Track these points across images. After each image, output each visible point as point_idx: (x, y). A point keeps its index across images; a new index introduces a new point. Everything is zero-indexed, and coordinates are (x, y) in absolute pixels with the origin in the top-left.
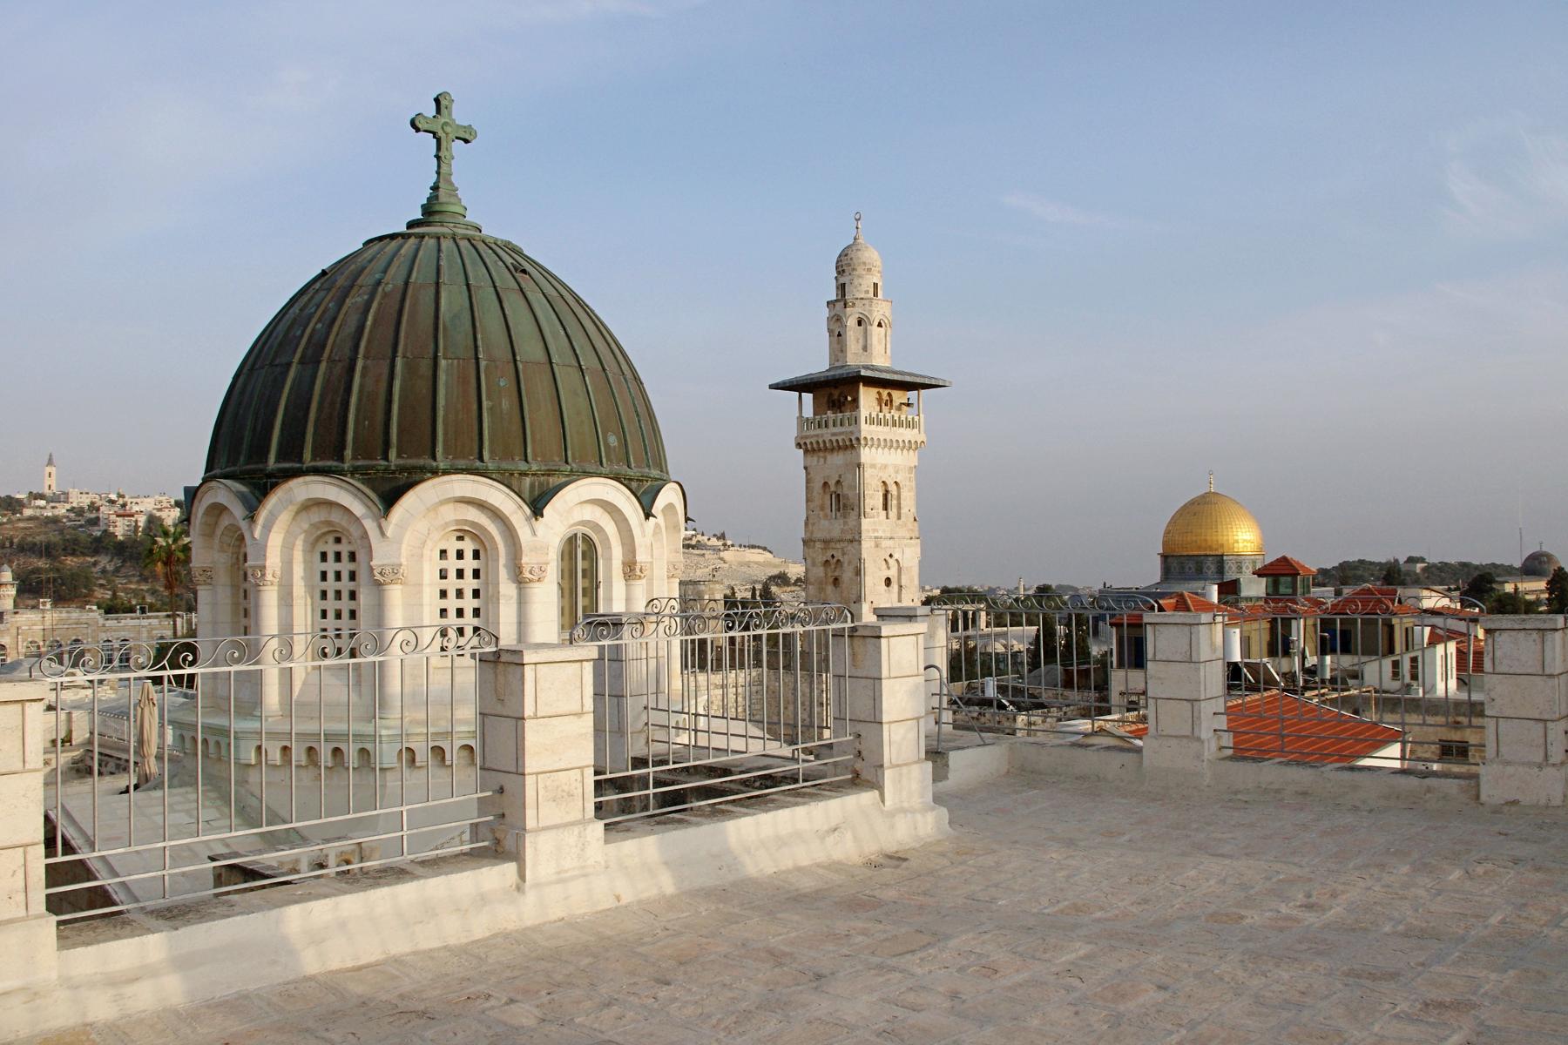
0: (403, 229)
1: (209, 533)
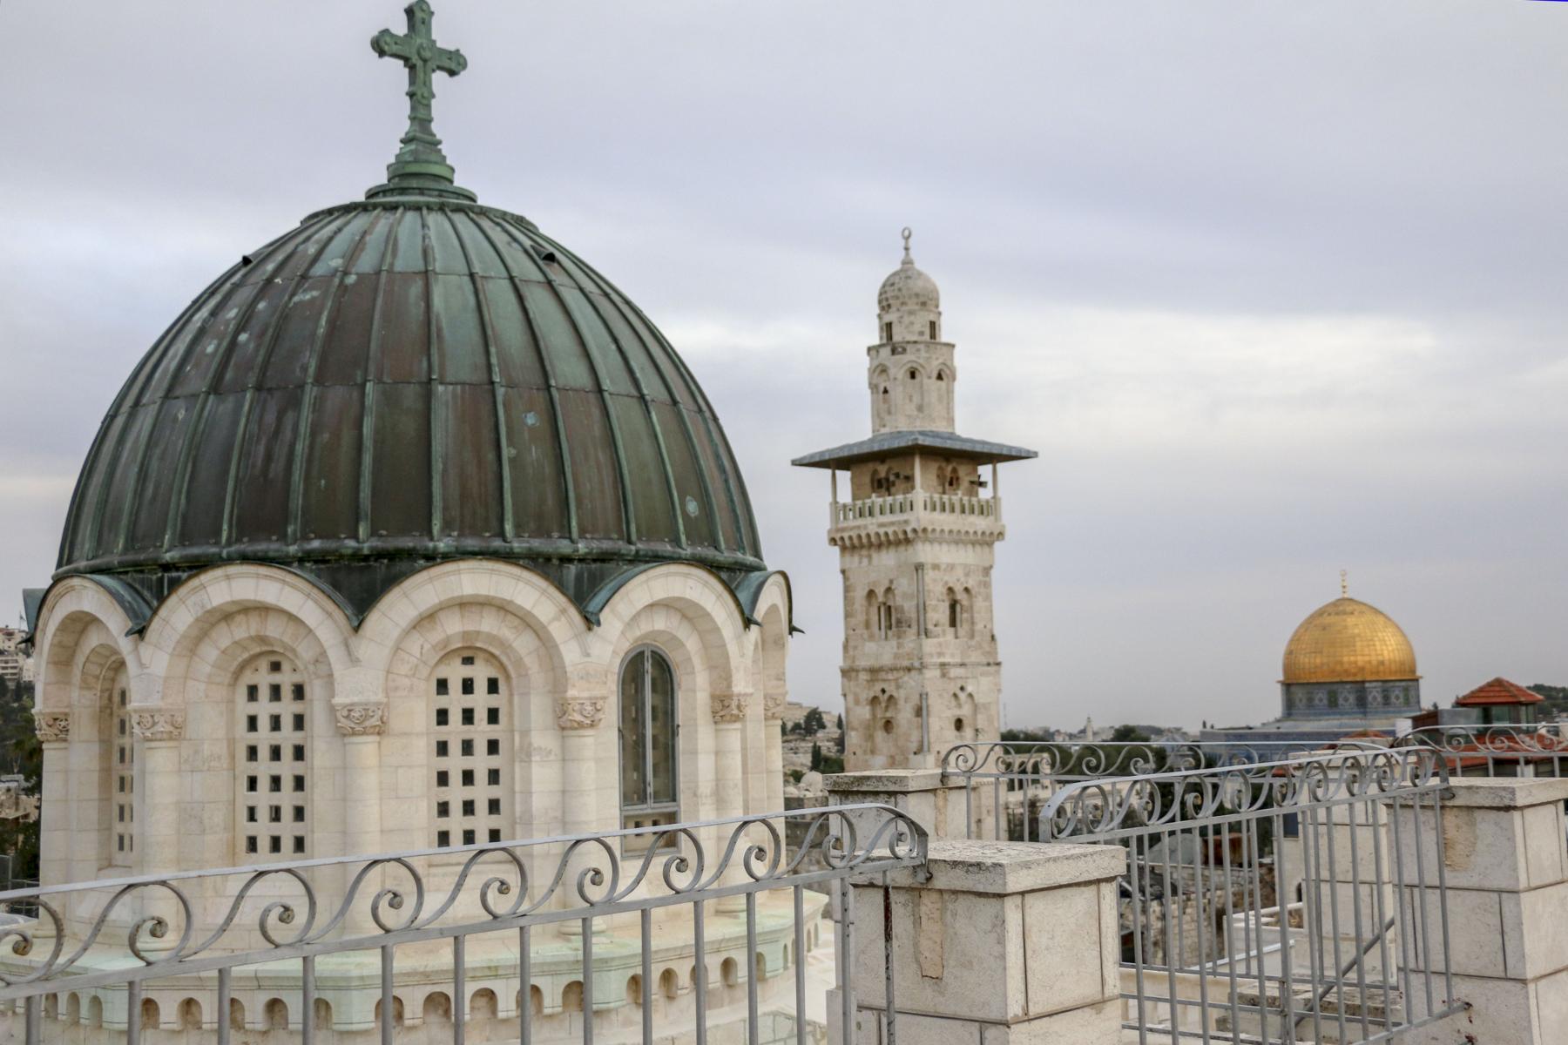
0: (361, 198)
1: (63, 660)
